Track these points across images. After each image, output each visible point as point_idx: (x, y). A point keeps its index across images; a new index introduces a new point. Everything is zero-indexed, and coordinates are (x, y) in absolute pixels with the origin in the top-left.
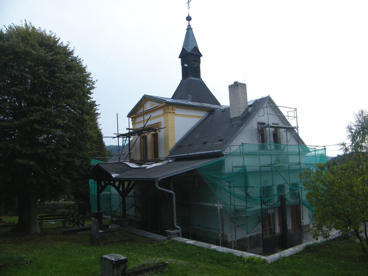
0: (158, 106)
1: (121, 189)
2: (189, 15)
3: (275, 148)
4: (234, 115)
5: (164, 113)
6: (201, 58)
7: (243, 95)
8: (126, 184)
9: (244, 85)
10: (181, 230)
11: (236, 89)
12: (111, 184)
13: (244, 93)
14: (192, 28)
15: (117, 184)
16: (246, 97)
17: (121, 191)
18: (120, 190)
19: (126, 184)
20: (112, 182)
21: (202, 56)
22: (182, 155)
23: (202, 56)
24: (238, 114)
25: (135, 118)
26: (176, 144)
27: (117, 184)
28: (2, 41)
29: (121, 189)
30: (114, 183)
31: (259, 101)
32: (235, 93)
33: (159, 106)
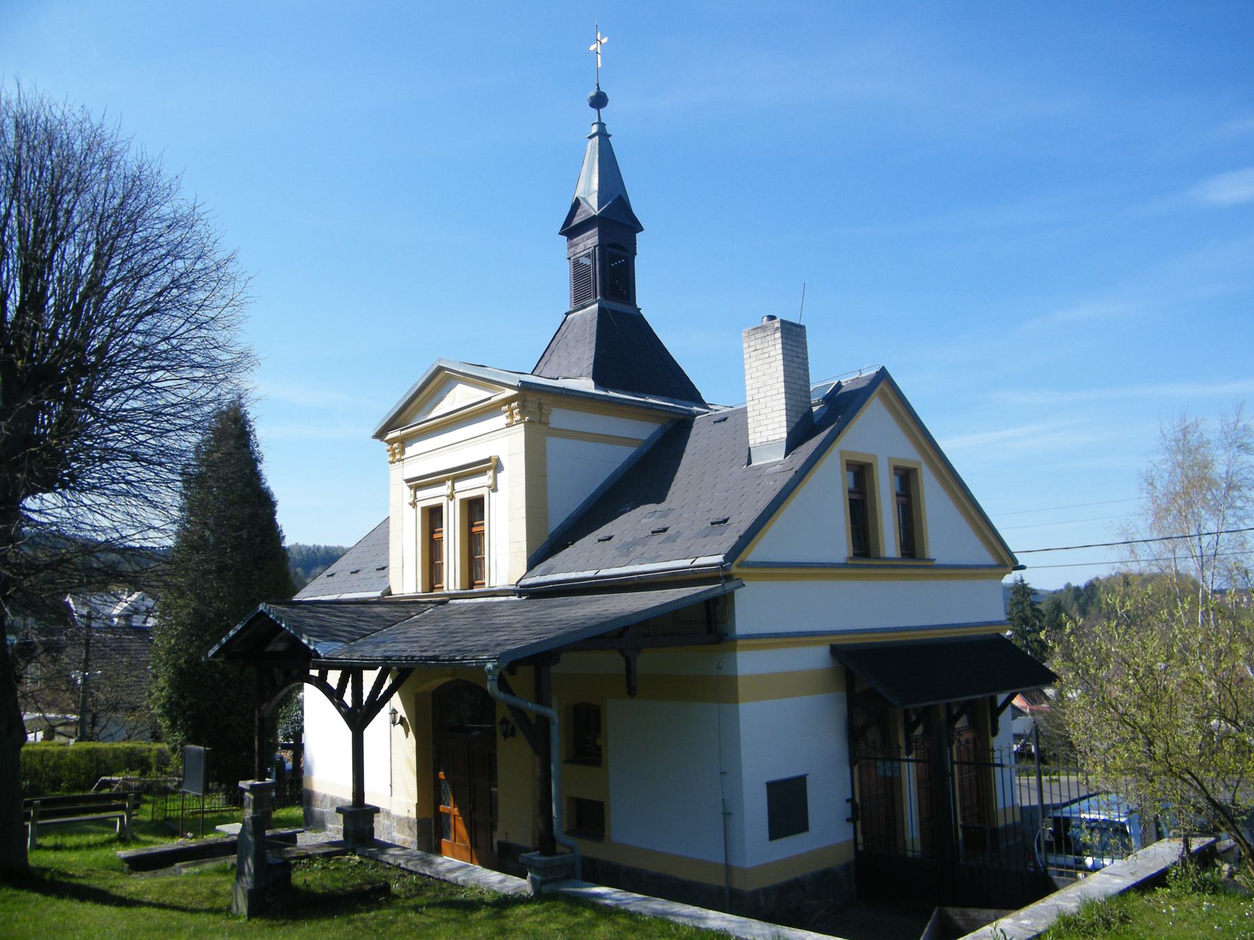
0: (489, 398)
1: (348, 698)
2: (598, 88)
3: (857, 552)
4: (763, 434)
5: (508, 426)
6: (639, 236)
7: (795, 365)
8: (369, 678)
9: (799, 329)
10: (364, 712)
11: (771, 343)
12: (311, 680)
13: (798, 357)
14: (609, 132)
15: (333, 678)
16: (807, 370)
17: (269, 649)
18: (345, 705)
19: (369, 678)
20: (314, 673)
21: (642, 229)
22: (573, 575)
23: (642, 229)
24: (776, 431)
25: (405, 442)
26: (552, 536)
27: (333, 678)
28: (107, 502)
29: (348, 698)
30: (323, 675)
31: (164, 551)
32: (767, 355)
33: (493, 400)
